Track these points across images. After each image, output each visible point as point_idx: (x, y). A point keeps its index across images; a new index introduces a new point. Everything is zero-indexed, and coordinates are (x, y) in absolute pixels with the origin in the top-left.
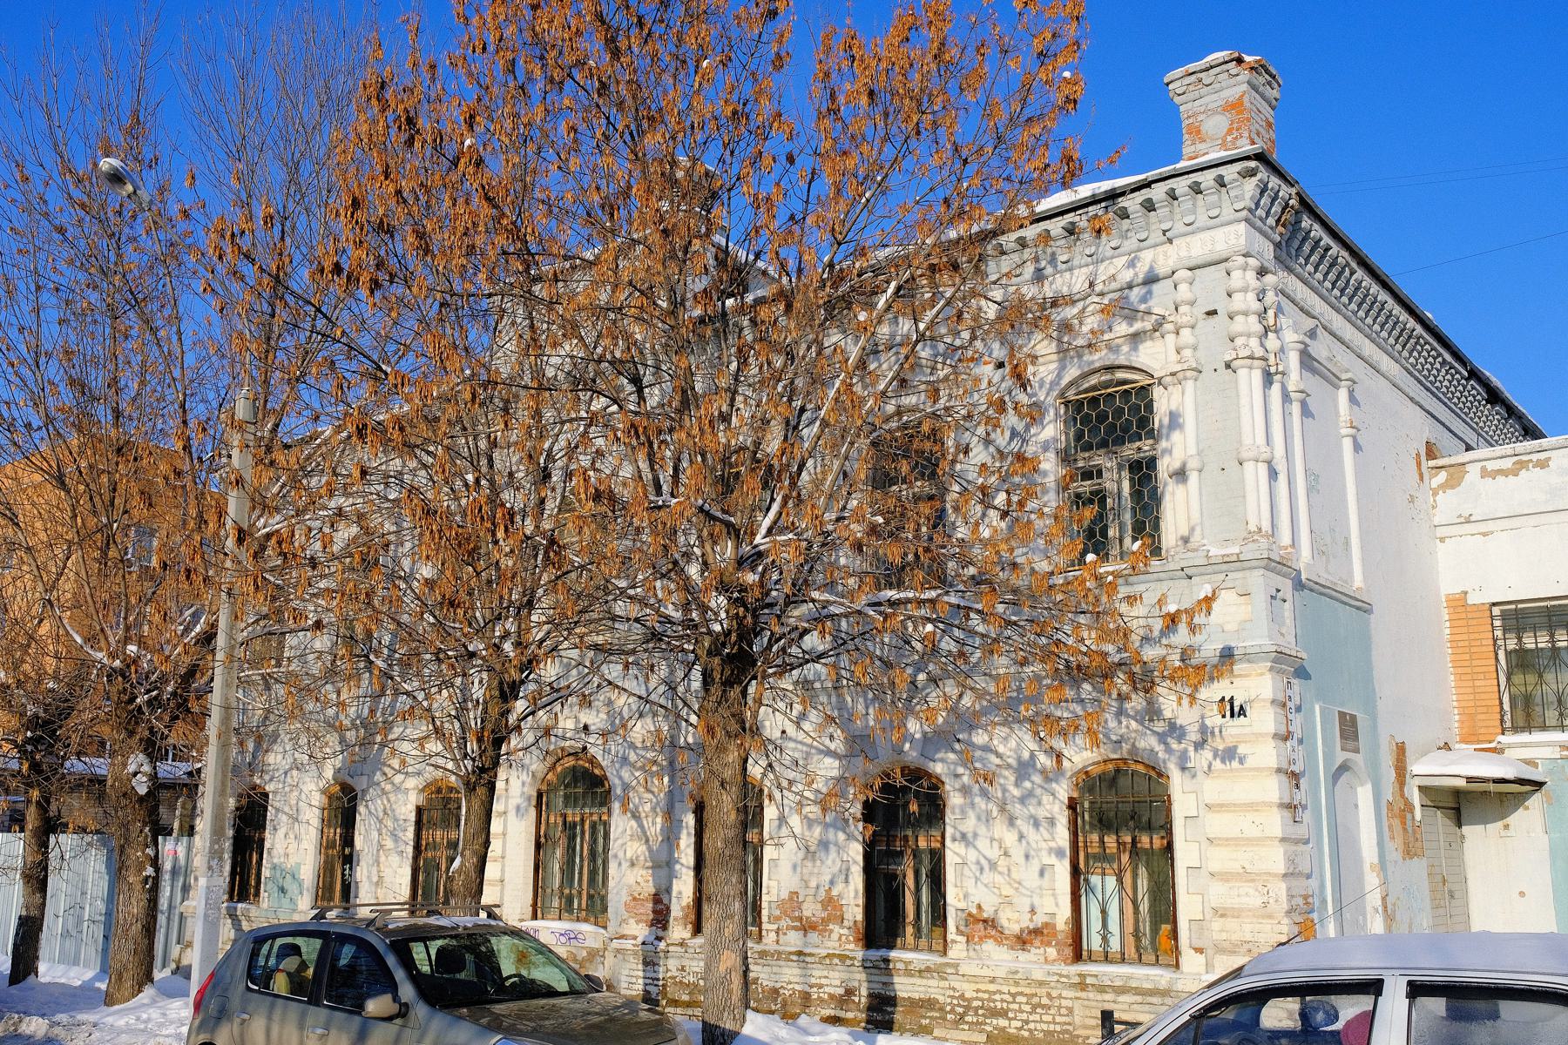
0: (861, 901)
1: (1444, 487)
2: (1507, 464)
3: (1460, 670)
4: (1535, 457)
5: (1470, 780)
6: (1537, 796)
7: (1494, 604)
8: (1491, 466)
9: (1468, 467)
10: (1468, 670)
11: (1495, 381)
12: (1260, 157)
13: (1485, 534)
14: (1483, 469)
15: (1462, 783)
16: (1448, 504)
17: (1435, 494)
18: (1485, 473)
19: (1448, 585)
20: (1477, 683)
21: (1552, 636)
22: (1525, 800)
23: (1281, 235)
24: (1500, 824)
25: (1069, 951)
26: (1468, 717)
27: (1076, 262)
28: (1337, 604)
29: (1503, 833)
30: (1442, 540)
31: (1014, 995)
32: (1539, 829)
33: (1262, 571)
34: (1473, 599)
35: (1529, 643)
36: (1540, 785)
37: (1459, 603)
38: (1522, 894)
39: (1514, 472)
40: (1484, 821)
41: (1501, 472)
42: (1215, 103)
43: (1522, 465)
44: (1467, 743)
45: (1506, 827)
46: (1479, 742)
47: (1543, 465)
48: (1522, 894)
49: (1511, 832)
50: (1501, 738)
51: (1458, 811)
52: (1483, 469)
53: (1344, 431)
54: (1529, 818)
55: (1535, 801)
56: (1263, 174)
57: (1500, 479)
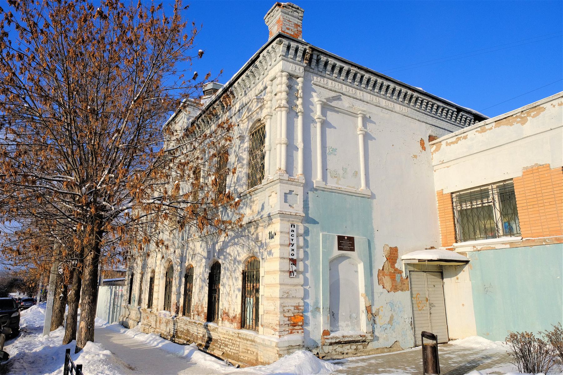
0: (207, 306)
1: (435, 151)
2: (454, 139)
3: (442, 219)
4: (463, 135)
5: (420, 260)
6: (467, 266)
7: (452, 193)
8: (449, 141)
9: (442, 143)
10: (444, 219)
11: (474, 111)
12: (279, 36)
13: (448, 167)
14: (447, 142)
15: (417, 262)
16: (436, 158)
17: (432, 154)
18: (448, 144)
19: (437, 188)
20: (447, 223)
21: (471, 203)
22: (463, 268)
23: (306, 63)
24: (455, 278)
25: (239, 325)
26: (445, 237)
27: (252, 87)
28: (345, 196)
29: (457, 281)
30: (435, 171)
31: (229, 339)
32: (468, 279)
33: (279, 184)
34: (445, 192)
35: (464, 206)
36: (467, 262)
37: (441, 193)
38: (463, 305)
39: (456, 142)
40: (451, 276)
41: (452, 143)
42: (275, 21)
43: (459, 139)
44: (444, 246)
45: (457, 279)
46: (448, 246)
47: (465, 138)
48: (463, 305)
49: (459, 281)
50: (455, 244)
51: (442, 273)
52: (447, 142)
53: (359, 133)
54: (465, 274)
55: (467, 268)
56: (286, 42)
57: (452, 145)
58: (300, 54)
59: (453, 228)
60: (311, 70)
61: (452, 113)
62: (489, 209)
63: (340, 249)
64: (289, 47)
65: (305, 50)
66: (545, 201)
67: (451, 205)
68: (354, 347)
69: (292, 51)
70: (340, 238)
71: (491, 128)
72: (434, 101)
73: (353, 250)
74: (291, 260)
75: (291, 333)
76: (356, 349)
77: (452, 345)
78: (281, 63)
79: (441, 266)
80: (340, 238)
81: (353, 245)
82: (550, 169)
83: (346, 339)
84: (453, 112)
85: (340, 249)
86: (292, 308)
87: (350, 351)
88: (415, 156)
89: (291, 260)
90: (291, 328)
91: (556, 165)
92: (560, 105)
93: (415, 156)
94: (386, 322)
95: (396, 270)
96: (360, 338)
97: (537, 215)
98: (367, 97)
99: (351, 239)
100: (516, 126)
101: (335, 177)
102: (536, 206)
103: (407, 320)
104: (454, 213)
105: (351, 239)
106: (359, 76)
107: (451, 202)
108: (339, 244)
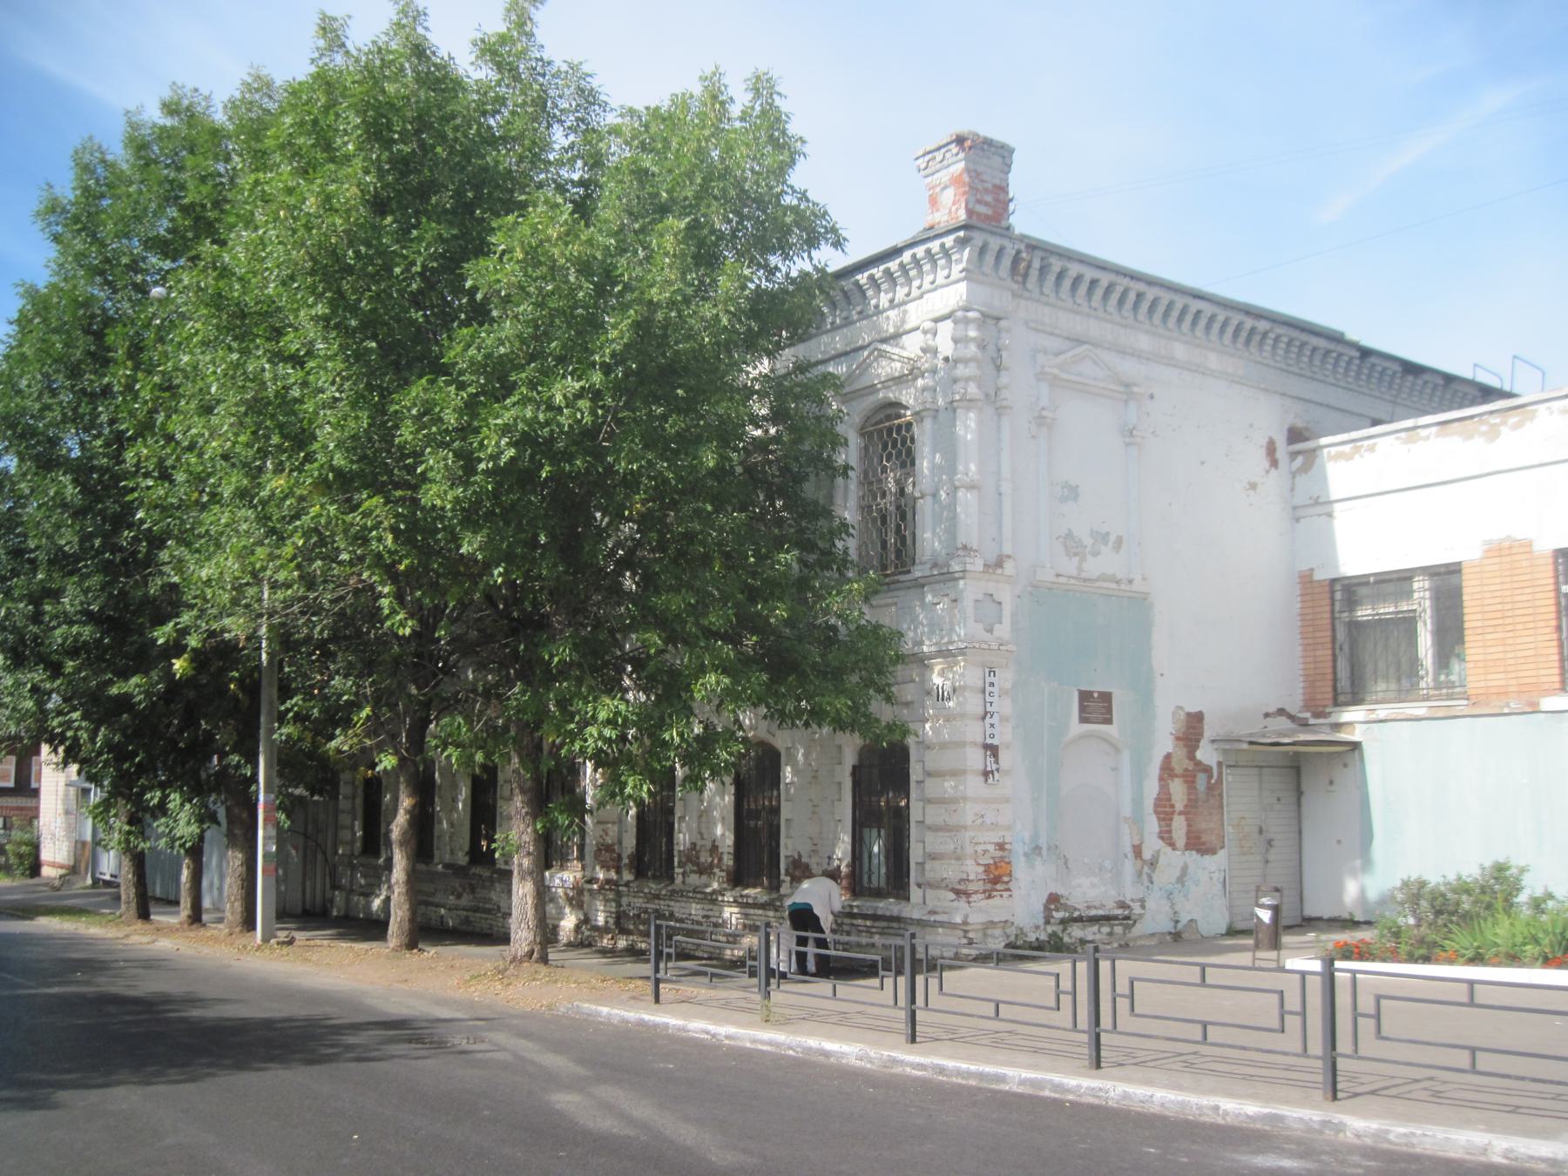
4: (1366, 443)
34: (1318, 576)
43: (1357, 449)
47: (1372, 449)
58: (1007, 262)
59: (1330, 664)
60: (1026, 294)
61: (1349, 362)
62: (1408, 624)
63: (1083, 720)
64: (983, 250)
65: (1018, 252)
66: (1518, 619)
67: (1328, 608)
68: (1106, 930)
69: (990, 258)
70: (1085, 696)
71: (1427, 438)
72: (1304, 337)
73: (1109, 721)
74: (987, 747)
75: (990, 897)
76: (1110, 934)
77: (1350, 724)
78: (964, 285)
79: (1297, 754)
80: (1085, 696)
81: (1109, 710)
82: (1530, 552)
83: (1093, 912)
84: (1351, 359)
85: (1083, 720)
86: (991, 848)
87: (1098, 937)
88: (1253, 486)
89: (987, 747)
90: (989, 886)
91: (1549, 541)
92: (1565, 411)
93: (1253, 486)
94: (1173, 880)
95: (1198, 763)
96: (1119, 912)
97: (1500, 649)
98: (1144, 342)
99: (1106, 697)
100: (1478, 443)
101: (1076, 554)
102: (1500, 629)
103: (1215, 876)
104: (1334, 630)
105: (1106, 697)
106: (1132, 296)
107: (1328, 601)
108: (1082, 709)
